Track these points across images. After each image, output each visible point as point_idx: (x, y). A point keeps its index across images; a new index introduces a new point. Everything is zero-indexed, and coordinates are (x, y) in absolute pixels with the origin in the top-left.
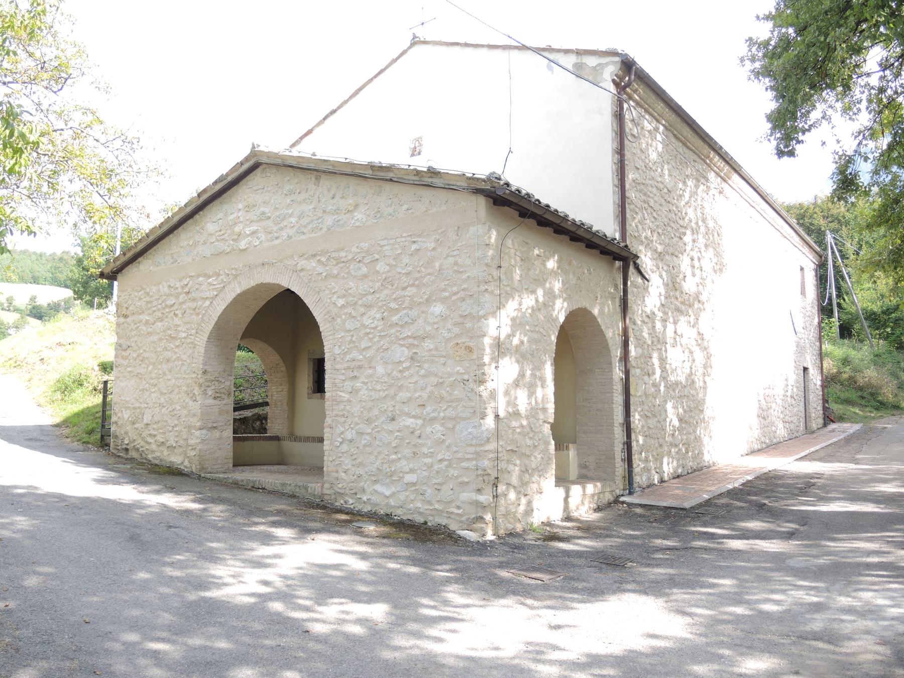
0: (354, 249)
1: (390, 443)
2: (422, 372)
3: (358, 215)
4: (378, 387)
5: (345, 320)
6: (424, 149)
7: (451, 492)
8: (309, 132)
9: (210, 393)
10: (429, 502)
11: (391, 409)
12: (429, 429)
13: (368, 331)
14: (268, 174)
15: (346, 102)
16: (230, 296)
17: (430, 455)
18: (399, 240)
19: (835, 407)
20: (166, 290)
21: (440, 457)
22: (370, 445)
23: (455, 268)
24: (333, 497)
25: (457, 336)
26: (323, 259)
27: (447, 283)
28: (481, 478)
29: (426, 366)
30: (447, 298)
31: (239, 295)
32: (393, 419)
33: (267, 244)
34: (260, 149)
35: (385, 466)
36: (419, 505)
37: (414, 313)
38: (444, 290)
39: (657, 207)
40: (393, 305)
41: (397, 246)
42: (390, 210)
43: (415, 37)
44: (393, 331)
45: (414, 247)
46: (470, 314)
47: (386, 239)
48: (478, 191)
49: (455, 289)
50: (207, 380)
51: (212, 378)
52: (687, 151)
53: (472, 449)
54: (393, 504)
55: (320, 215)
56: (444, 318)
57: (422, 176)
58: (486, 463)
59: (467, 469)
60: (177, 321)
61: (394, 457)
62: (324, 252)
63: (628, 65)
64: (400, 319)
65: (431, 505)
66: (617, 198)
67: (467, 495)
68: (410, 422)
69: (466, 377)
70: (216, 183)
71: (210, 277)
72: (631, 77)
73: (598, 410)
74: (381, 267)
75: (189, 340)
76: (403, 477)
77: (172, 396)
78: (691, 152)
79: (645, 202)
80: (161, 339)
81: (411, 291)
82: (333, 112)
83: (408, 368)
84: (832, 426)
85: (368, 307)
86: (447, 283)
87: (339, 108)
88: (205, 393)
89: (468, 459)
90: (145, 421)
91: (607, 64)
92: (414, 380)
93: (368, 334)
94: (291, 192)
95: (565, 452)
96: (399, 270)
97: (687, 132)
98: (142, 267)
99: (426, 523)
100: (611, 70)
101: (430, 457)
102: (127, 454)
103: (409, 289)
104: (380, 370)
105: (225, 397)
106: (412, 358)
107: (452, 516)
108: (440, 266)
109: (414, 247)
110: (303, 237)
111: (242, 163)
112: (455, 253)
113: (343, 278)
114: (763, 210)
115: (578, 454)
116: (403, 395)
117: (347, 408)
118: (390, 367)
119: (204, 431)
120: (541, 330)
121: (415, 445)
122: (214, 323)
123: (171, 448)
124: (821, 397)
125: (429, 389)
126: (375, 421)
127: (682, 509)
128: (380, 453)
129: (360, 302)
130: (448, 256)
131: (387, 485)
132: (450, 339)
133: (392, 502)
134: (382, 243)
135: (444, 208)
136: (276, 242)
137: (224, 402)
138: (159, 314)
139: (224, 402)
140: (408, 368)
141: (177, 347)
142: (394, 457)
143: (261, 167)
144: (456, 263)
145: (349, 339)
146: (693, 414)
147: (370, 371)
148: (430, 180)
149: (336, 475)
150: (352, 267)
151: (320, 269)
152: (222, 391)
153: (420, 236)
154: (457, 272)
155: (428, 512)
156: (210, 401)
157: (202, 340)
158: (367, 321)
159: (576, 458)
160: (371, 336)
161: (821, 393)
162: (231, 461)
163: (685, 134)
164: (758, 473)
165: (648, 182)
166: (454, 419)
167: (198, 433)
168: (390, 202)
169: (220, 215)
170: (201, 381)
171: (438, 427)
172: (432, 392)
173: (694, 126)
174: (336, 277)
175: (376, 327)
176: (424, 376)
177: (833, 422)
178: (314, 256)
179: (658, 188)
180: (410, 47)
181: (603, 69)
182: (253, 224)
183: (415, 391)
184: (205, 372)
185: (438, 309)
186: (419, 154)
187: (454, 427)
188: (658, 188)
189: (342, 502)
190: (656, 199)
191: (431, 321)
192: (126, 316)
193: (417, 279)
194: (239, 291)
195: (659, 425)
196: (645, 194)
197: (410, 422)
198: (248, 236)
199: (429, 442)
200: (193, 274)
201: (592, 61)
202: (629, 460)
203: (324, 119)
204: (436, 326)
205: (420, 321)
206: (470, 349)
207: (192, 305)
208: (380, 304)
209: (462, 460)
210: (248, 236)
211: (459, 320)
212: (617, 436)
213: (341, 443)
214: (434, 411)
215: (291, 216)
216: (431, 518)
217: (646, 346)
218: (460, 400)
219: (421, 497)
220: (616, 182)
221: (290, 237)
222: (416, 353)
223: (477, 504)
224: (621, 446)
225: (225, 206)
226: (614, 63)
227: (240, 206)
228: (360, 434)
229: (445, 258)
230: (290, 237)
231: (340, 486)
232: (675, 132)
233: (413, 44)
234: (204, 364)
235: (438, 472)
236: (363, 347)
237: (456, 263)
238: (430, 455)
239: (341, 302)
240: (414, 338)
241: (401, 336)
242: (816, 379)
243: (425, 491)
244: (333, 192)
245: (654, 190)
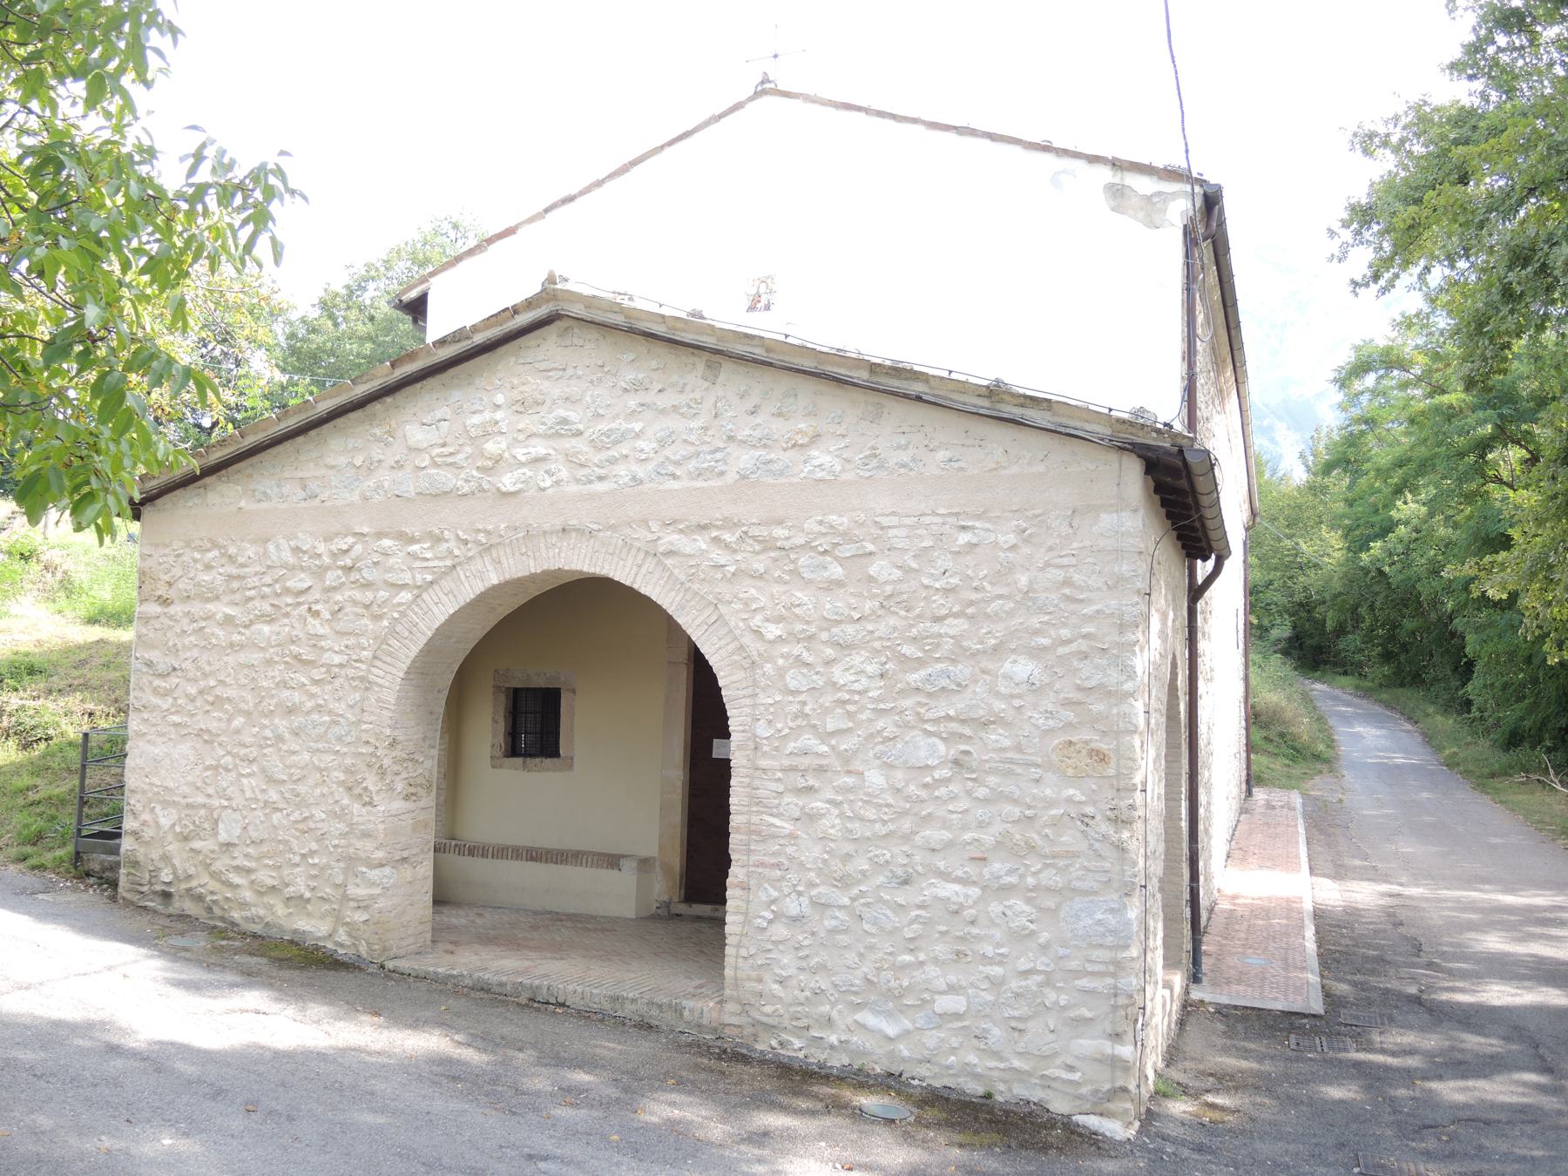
16: (470, 589)
18: (927, 520)
23: (1067, 591)
30: (1045, 649)
45: (964, 538)
47: (894, 513)
54: (906, 1053)
61: (908, 958)
67: (1089, 1044)
91: (1174, 195)
92: (963, 805)
94: (637, 387)
105: (421, 792)
109: (964, 538)
110: (674, 485)
111: (515, 310)
119: (387, 870)
136: (600, 487)
142: (908, 958)
144: (1067, 582)
153: (979, 517)
155: (995, 1074)
169: (442, 411)
180: (751, 99)
186: (767, 308)
203: (547, 211)
204: (1017, 703)
206: (1101, 757)
233: (757, 95)
237: (1067, 582)
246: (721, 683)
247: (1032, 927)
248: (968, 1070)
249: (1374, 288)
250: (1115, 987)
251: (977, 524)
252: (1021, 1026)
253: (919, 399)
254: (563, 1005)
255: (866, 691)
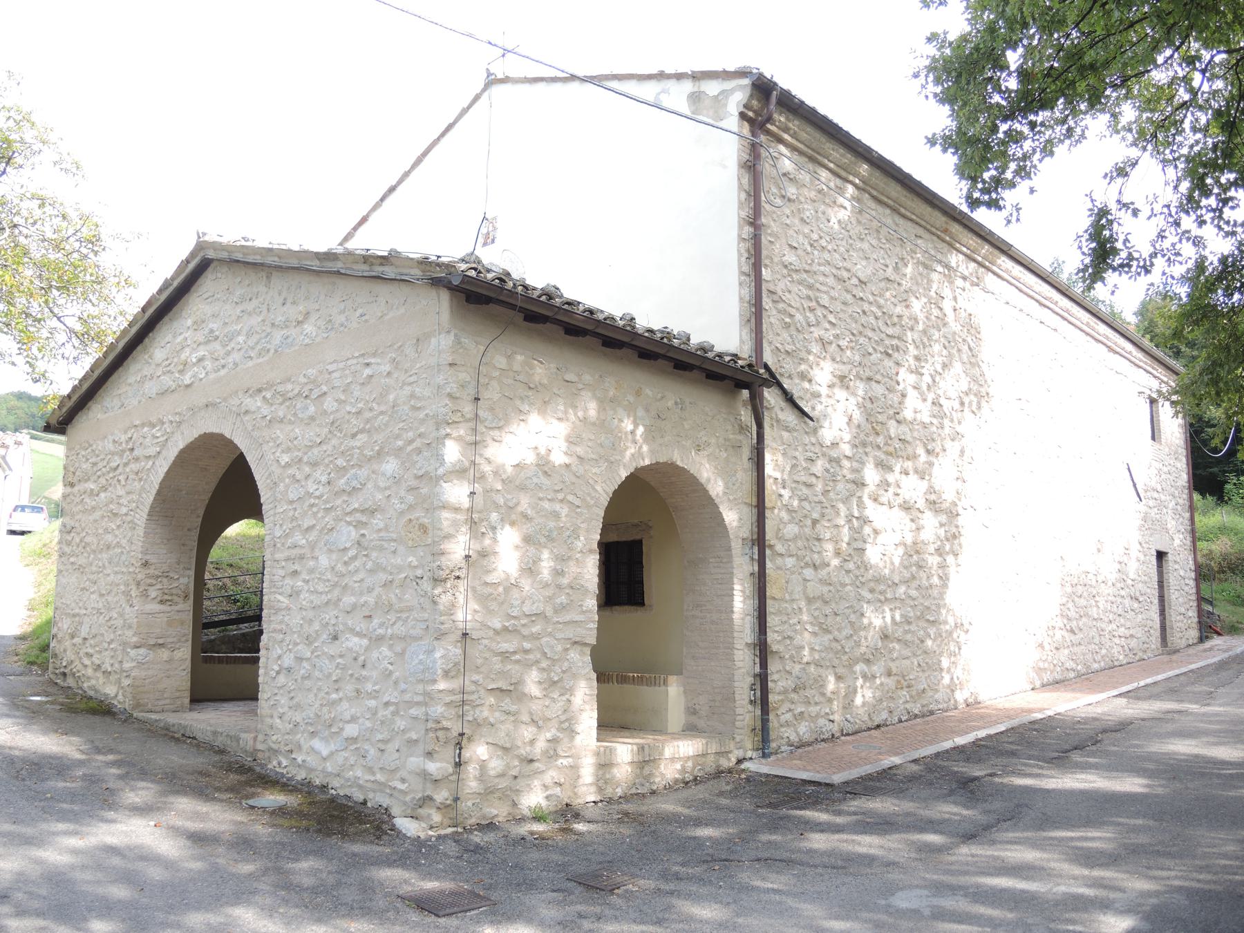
0: (302, 380)
1: (330, 675)
2: (369, 565)
3: (308, 328)
4: (320, 588)
5: (287, 487)
6: (499, 235)
7: (397, 755)
8: (364, 220)
9: (153, 594)
10: (370, 770)
11: (333, 622)
12: (375, 655)
13: (312, 501)
14: (219, 275)
15: (406, 174)
16: (172, 453)
17: (374, 695)
18: (349, 362)
19: (1223, 611)
20: (111, 447)
21: (386, 699)
22: (308, 677)
23: (412, 403)
24: (267, 754)
25: (411, 507)
26: (268, 395)
27: (401, 425)
28: (431, 735)
29: (374, 554)
30: (401, 449)
31: (182, 452)
32: (335, 638)
33: (212, 376)
34: (206, 238)
35: (325, 709)
36: (359, 773)
37: (363, 473)
38: (398, 437)
39: (838, 306)
40: (341, 462)
41: (347, 372)
42: (342, 318)
43: (489, 74)
44: (339, 502)
45: (368, 371)
46: (427, 473)
47: (335, 361)
48: (436, 282)
49: (410, 434)
50: (148, 576)
51: (157, 573)
52: (901, 221)
53: (420, 688)
54: (330, 769)
55: (269, 330)
56: (397, 481)
57: (372, 264)
58: (438, 710)
59: (415, 718)
60: (121, 492)
61: (334, 696)
62: (270, 385)
63: (763, 88)
64: (347, 483)
65: (373, 774)
66: (747, 293)
67: (415, 761)
68: (354, 642)
69: (419, 572)
70: (160, 291)
71: (154, 426)
72: (771, 109)
73: (713, 622)
74: (329, 404)
75: (129, 518)
76: (342, 729)
77: (110, 599)
78: (909, 224)
79: (809, 298)
80: (103, 517)
81: (362, 438)
82: (392, 189)
83: (354, 558)
84: (1217, 641)
85: (314, 465)
86: (401, 425)
87: (400, 182)
88: (144, 594)
89: (418, 703)
90: (83, 634)
91: (732, 91)
92: (360, 576)
93: (312, 505)
94: (242, 300)
95: (663, 688)
96: (348, 408)
97: (895, 190)
98: (91, 414)
99: (365, 803)
100: (738, 97)
101: (375, 698)
102: (64, 680)
103: (359, 436)
104: (324, 561)
105: (180, 600)
106: (359, 543)
107: (396, 794)
108: (395, 400)
109: (368, 371)
110: (250, 364)
111: (187, 261)
112: (412, 379)
113: (291, 422)
114: (1067, 311)
115: (685, 692)
116: (348, 600)
117: (286, 619)
118: (334, 556)
119: (142, 651)
120: (570, 498)
121: (358, 679)
122: (154, 492)
123: (107, 673)
124: (1194, 597)
125: (378, 590)
126: (315, 640)
127: (827, 785)
128: (319, 689)
129: (305, 459)
130: (404, 384)
131: (325, 740)
132: (402, 513)
133: (329, 767)
134: (331, 368)
135: (402, 310)
136: (223, 372)
137: (177, 608)
138: (103, 481)
139: (177, 608)
140: (354, 558)
141: (119, 527)
142: (334, 696)
143: (212, 266)
144: (412, 396)
145: (291, 514)
146: (913, 627)
147: (311, 563)
148: (381, 269)
149: (269, 721)
150: (299, 405)
151: (265, 410)
152: (174, 591)
153: (374, 355)
154: (415, 408)
155: (369, 785)
156: (156, 607)
157: (141, 517)
158: (311, 487)
159: (683, 699)
160: (315, 509)
161: (1194, 591)
162: (187, 694)
163: (894, 194)
164: (1015, 722)
165: (815, 268)
166: (402, 638)
167: (133, 653)
168: (342, 306)
169: (169, 338)
170: (140, 577)
171: (385, 650)
172: (379, 597)
173: (906, 181)
174: (281, 421)
175: (322, 496)
176: (371, 571)
177: (1219, 634)
178: (259, 391)
179: (840, 280)
180: (484, 90)
181: (727, 98)
182: (201, 347)
183: (361, 594)
184: (146, 564)
185: (390, 466)
186: (493, 241)
187: (403, 653)
188: (840, 280)
189: (275, 763)
190: (833, 293)
191: (382, 485)
192: (72, 485)
193: (368, 421)
194: (181, 445)
195: (834, 644)
196: (810, 287)
197: (354, 642)
198: (194, 364)
199: (375, 674)
200: (137, 423)
201: (712, 88)
202: (763, 702)
203: (382, 199)
204: (387, 493)
205: (369, 485)
206: (424, 529)
207: (134, 466)
208: (326, 461)
209: (411, 704)
210: (194, 364)
211: (414, 483)
212: (739, 664)
213: (278, 673)
214: (381, 625)
215: (239, 334)
216: (371, 795)
217: (809, 522)
218: (410, 609)
219: (362, 761)
220: (746, 269)
221: (236, 365)
222: (363, 535)
223: (425, 775)
224: (750, 680)
225: (175, 324)
226: (741, 87)
227: (189, 322)
228: (300, 659)
229: (401, 388)
230: (236, 365)
231: (274, 738)
232: (875, 193)
233: (487, 86)
234: (145, 553)
235: (383, 722)
236: (306, 526)
237: (412, 396)
238: (374, 695)
239: (285, 459)
240: (363, 511)
241: (348, 510)
242: (1182, 571)
243: (367, 751)
244: (284, 294)
245: (831, 281)
246: (262, 501)
247: (390, 667)
248: (355, 783)
249: (1067, 142)
250: (427, 714)
251: (373, 361)
252: (383, 747)
253: (338, 273)
254: (194, 738)
255: (322, 496)
